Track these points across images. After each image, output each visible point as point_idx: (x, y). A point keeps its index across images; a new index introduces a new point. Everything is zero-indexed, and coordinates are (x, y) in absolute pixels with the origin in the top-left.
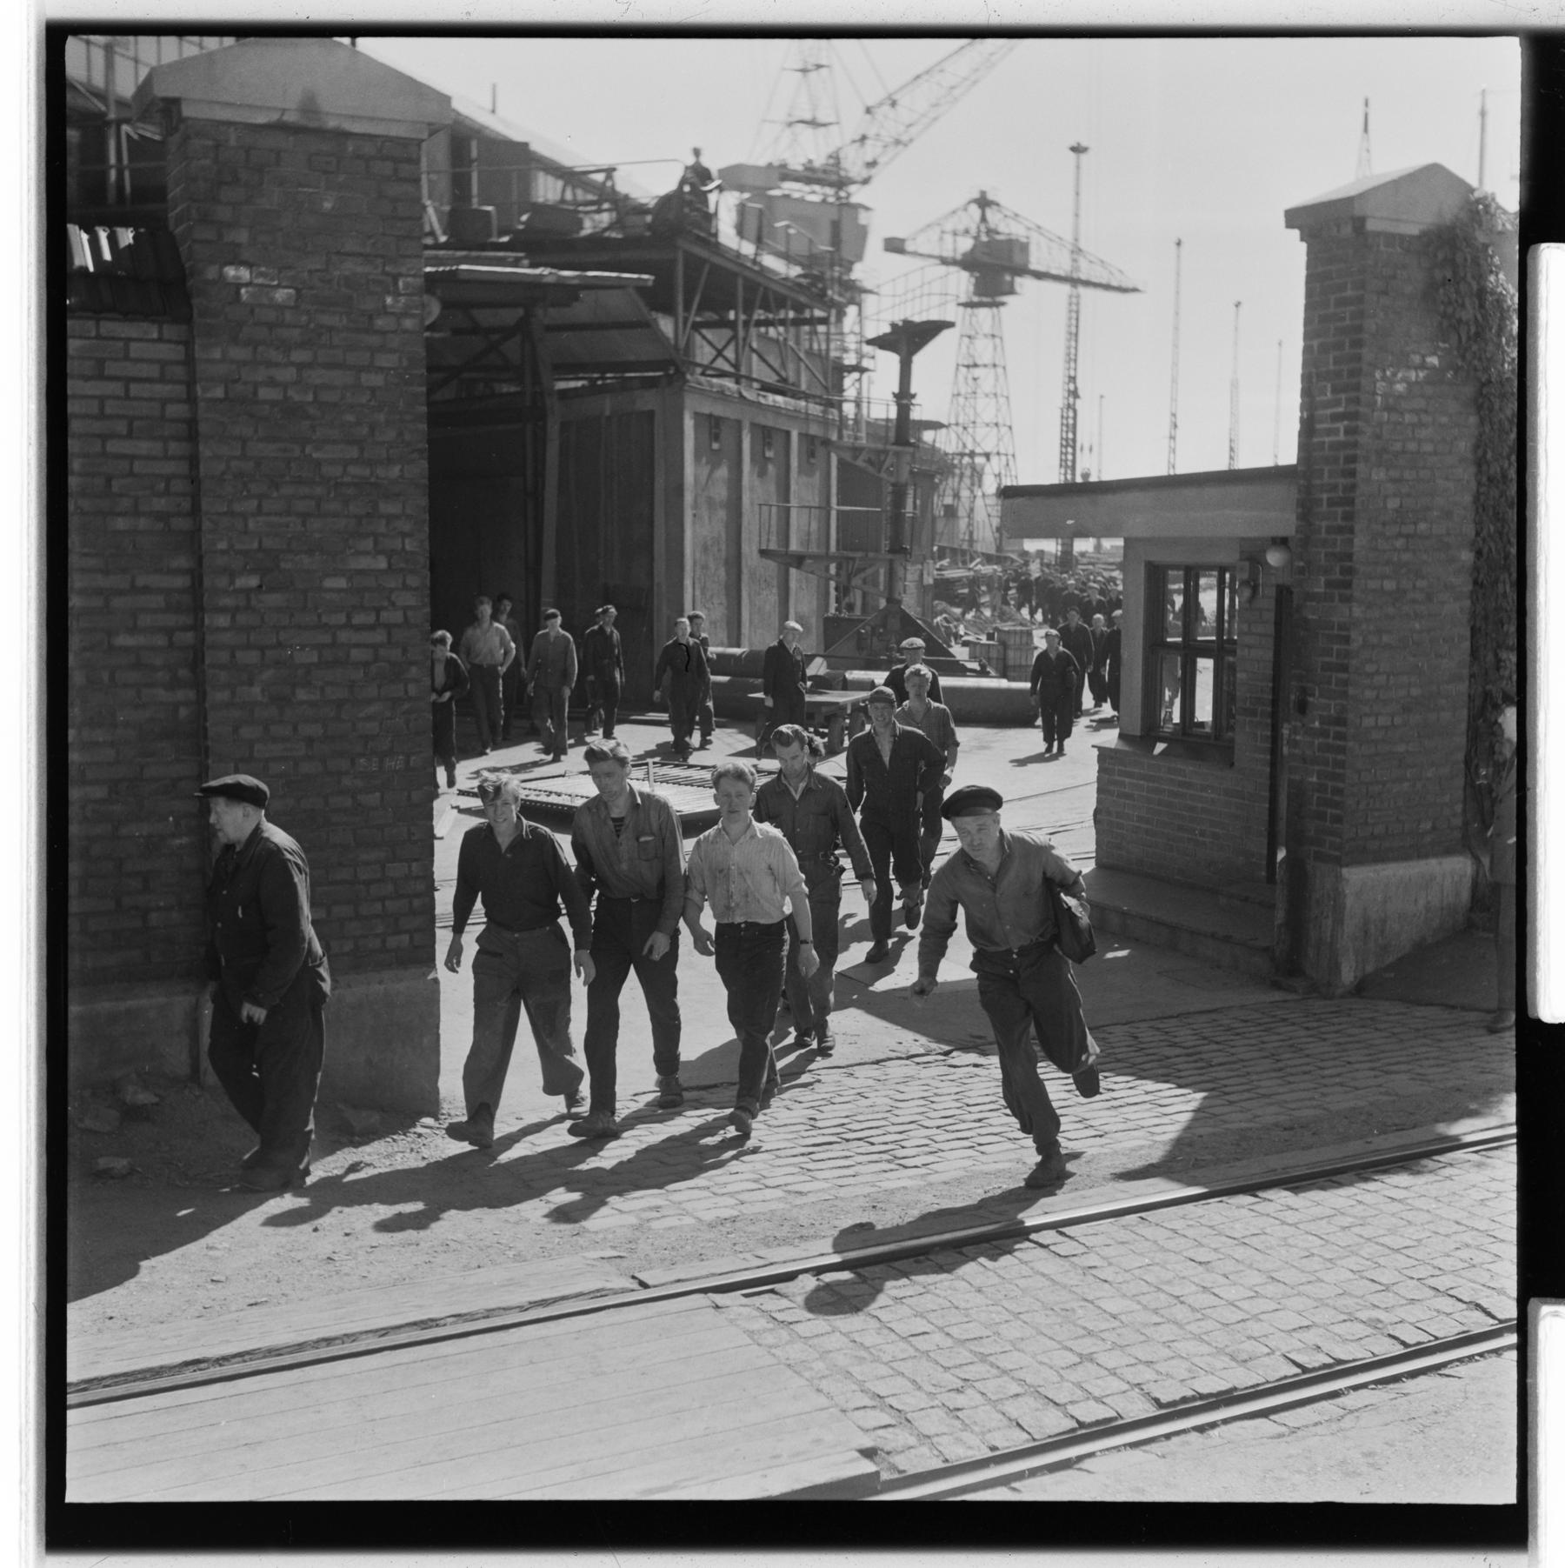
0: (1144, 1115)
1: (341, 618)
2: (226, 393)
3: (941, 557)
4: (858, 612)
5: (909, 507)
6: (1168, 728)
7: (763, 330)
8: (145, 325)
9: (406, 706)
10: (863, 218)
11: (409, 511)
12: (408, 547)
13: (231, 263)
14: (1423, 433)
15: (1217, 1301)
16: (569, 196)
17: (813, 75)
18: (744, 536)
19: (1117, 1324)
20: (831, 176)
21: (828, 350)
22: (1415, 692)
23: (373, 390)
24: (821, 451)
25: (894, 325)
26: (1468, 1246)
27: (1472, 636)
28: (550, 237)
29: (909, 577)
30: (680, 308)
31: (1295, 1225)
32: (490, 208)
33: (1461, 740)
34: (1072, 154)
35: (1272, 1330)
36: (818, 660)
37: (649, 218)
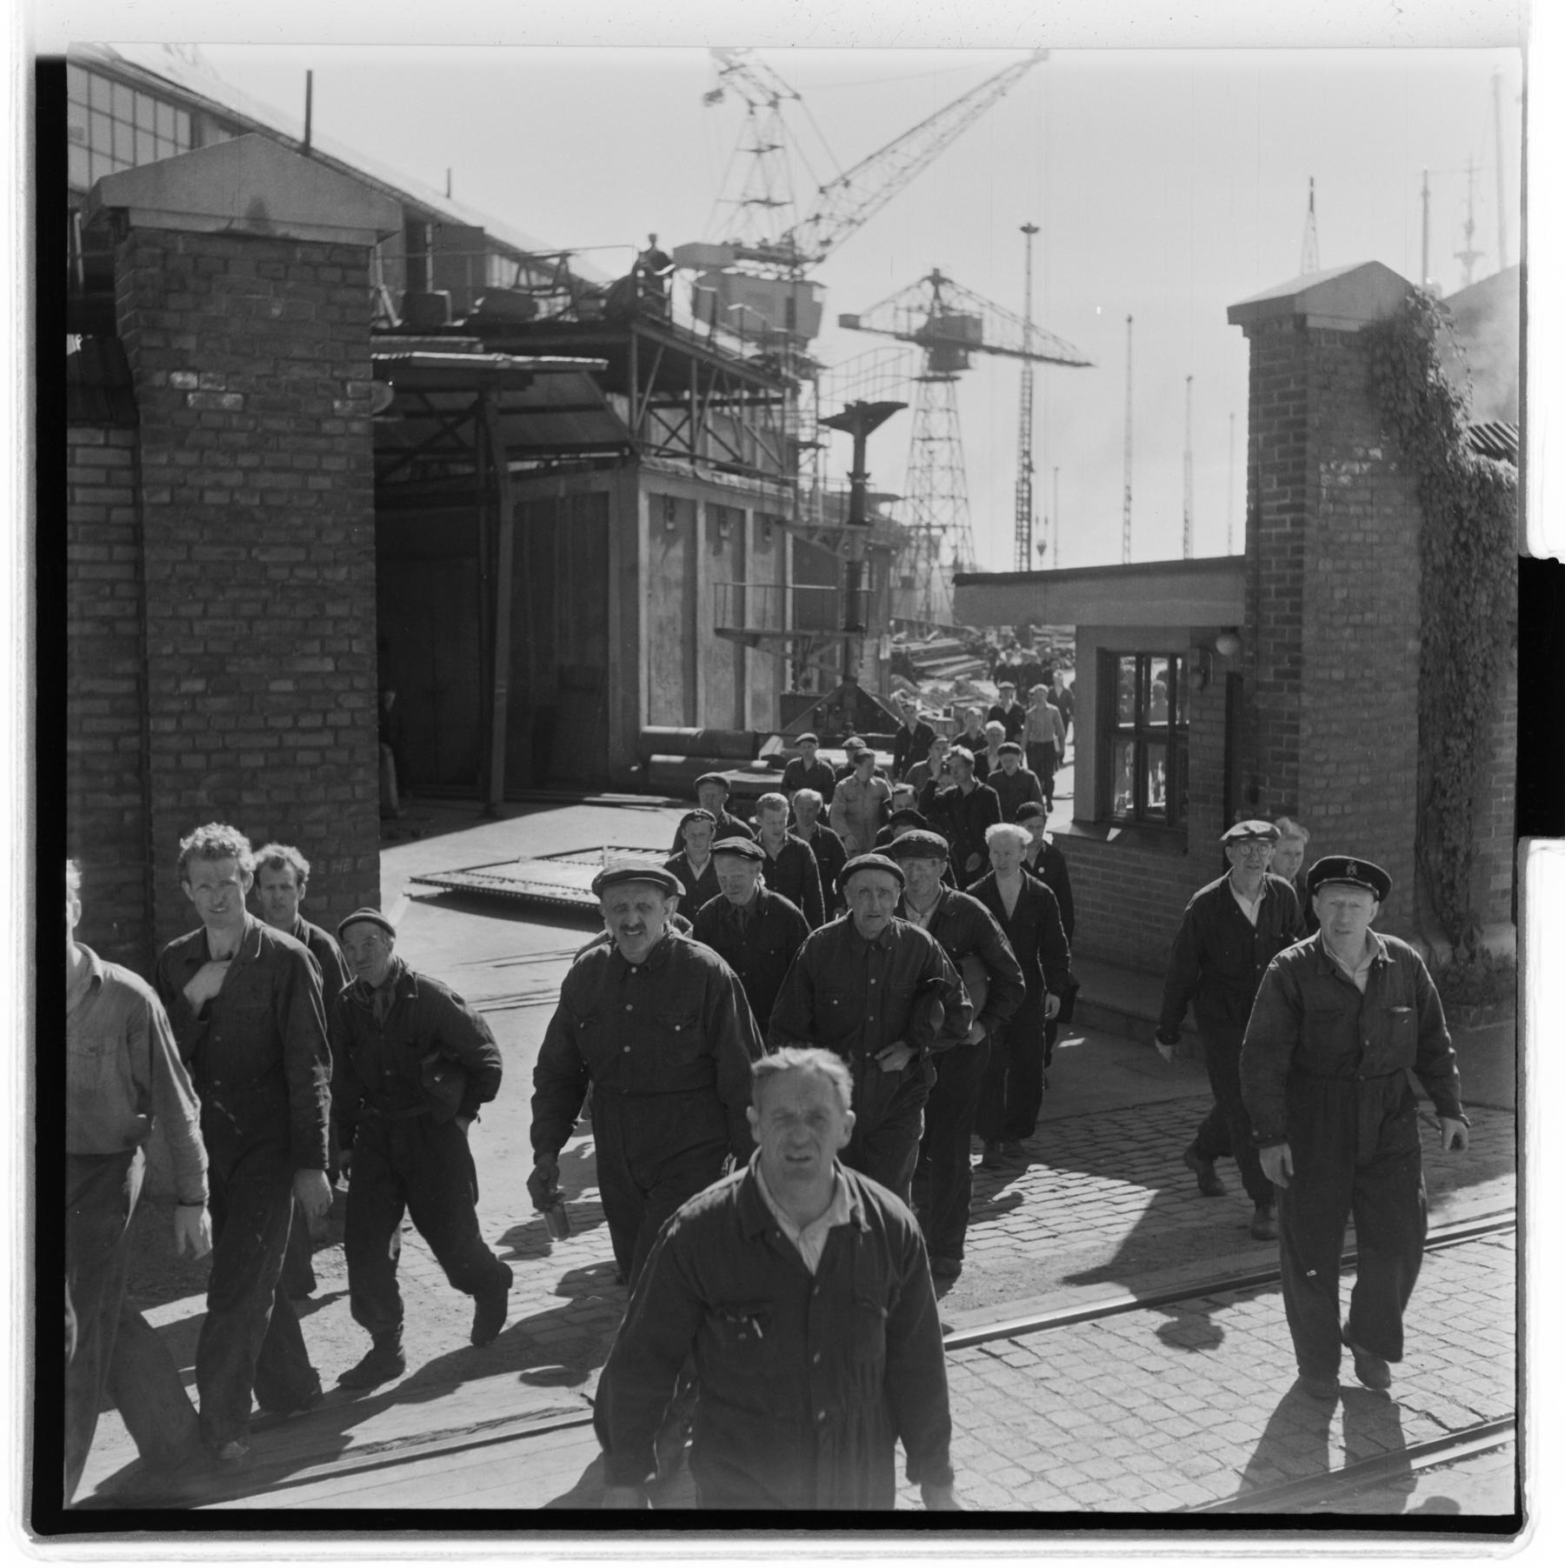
0: (1096, 1214)
1: (287, 721)
2: (172, 496)
3: (899, 629)
4: (814, 689)
5: (864, 586)
6: (1122, 814)
7: (718, 409)
8: (91, 431)
9: (353, 809)
10: (818, 296)
11: (356, 612)
12: (355, 650)
13: (177, 369)
14: (1368, 525)
15: (1169, 1413)
16: (523, 280)
17: (767, 156)
18: (700, 614)
19: (1068, 1438)
20: (786, 254)
21: (783, 427)
22: (1364, 780)
23: (320, 493)
24: (776, 530)
25: (847, 406)
26: (1418, 1351)
27: (1420, 725)
28: (505, 322)
29: (866, 652)
30: (635, 389)
31: (1247, 1331)
32: (444, 293)
33: (1412, 828)
34: (1023, 235)
35: (1223, 1443)
36: (774, 740)
37: (603, 303)
